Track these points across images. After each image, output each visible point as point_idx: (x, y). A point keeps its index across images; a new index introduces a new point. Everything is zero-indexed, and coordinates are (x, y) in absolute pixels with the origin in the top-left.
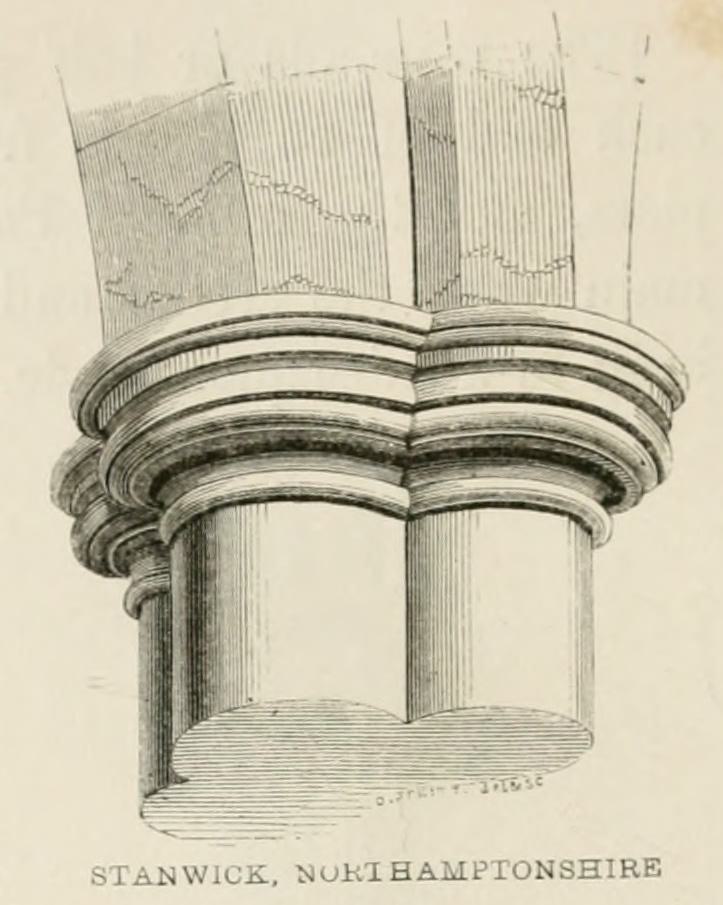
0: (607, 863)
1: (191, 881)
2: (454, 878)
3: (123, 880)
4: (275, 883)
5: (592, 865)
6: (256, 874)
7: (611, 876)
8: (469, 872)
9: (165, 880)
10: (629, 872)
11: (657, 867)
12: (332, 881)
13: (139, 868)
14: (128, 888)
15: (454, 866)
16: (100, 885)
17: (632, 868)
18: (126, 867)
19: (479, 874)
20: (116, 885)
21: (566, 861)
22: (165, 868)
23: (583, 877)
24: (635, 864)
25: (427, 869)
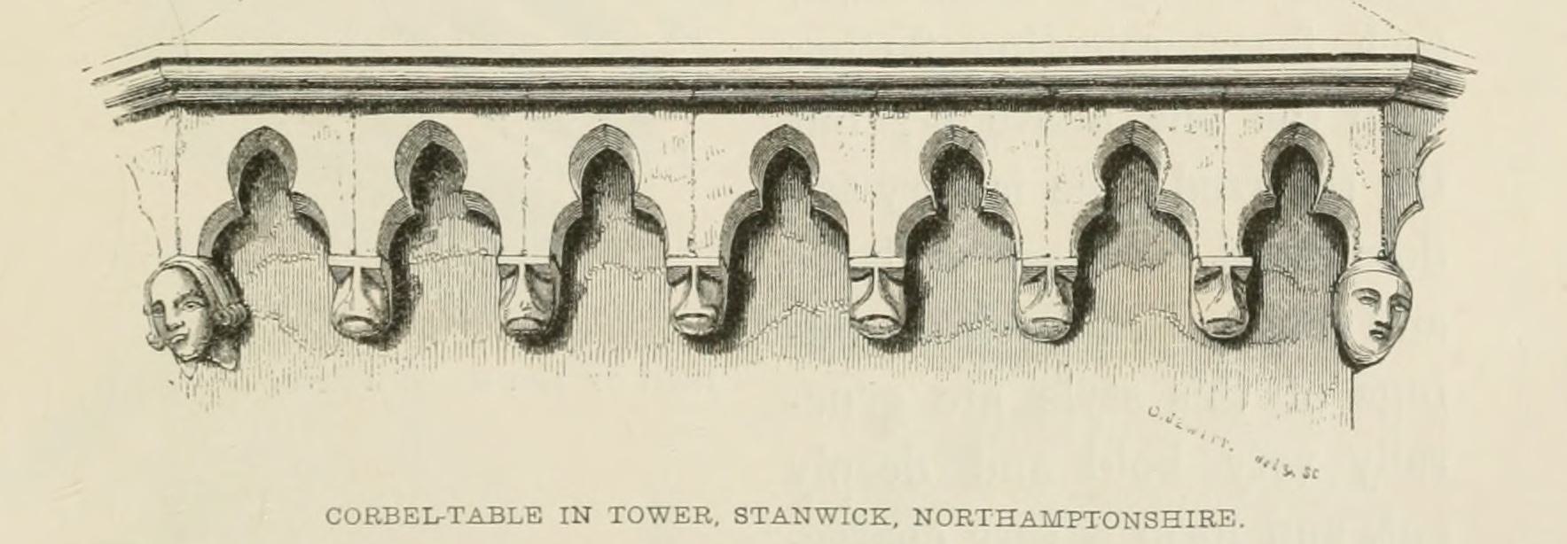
0: (1188, 514)
1: (822, 522)
2: (1052, 526)
3: (459, 519)
4: (896, 525)
5: (1174, 515)
7: (1190, 526)
8: (1065, 519)
9: (800, 519)
10: (1207, 523)
11: (538, 515)
12: (641, 520)
14: (992, 528)
15: (1052, 514)
16: (1153, 528)
17: (374, 516)
18: (766, 508)
19: (1074, 523)
23: (1165, 526)
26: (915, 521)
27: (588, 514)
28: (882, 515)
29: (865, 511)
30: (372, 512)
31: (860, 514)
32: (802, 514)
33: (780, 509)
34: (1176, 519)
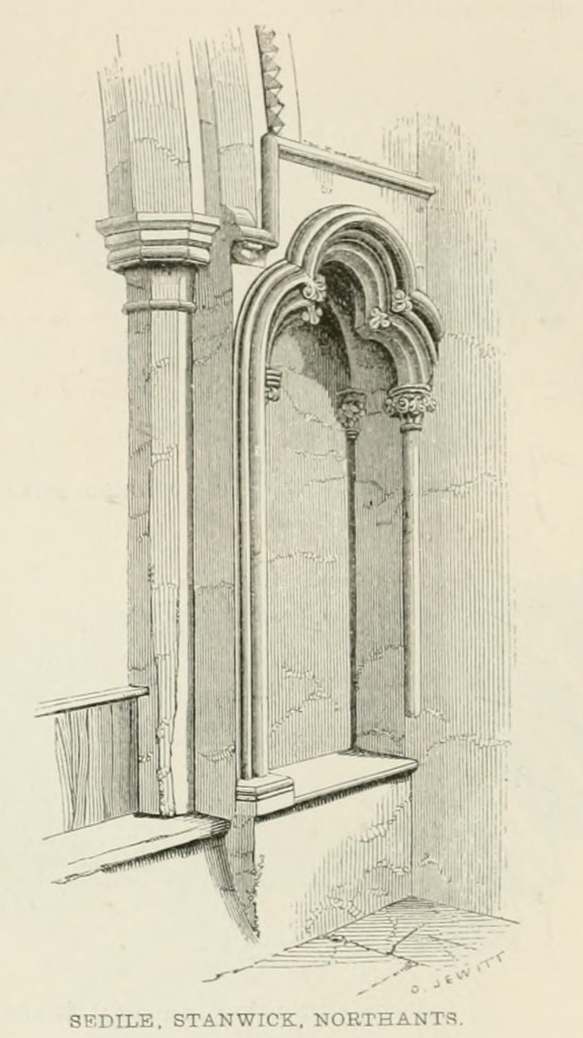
1: (243, 1024)
6: (288, 1020)
11: (150, 1021)
13: (207, 1015)
14: (375, 1028)
18: (198, 1015)
20: (434, 1024)
21: (74, 1016)
22: (419, 1014)
24: (358, 1016)
25: (404, 1017)
26: (316, 1023)
27: (425, 1018)
28: (291, 1019)
29: (277, 1016)
30: (354, 1016)
31: (273, 1017)
32: (226, 1019)
33: (209, 1016)
34: (389, 1019)
